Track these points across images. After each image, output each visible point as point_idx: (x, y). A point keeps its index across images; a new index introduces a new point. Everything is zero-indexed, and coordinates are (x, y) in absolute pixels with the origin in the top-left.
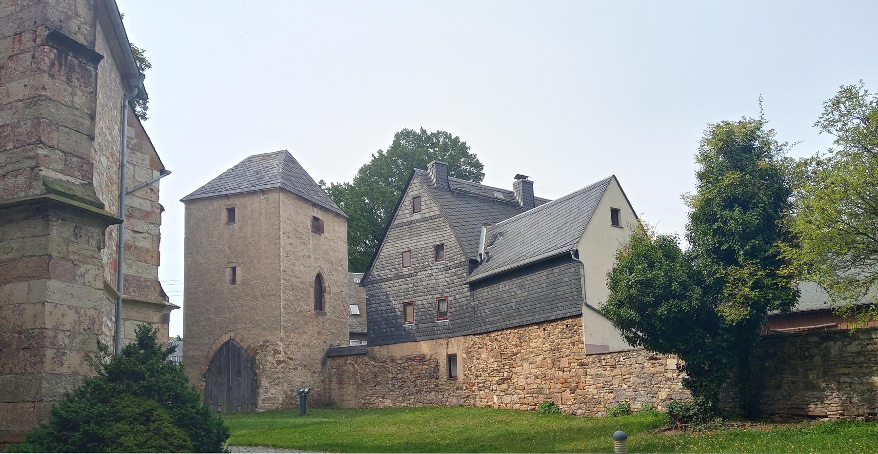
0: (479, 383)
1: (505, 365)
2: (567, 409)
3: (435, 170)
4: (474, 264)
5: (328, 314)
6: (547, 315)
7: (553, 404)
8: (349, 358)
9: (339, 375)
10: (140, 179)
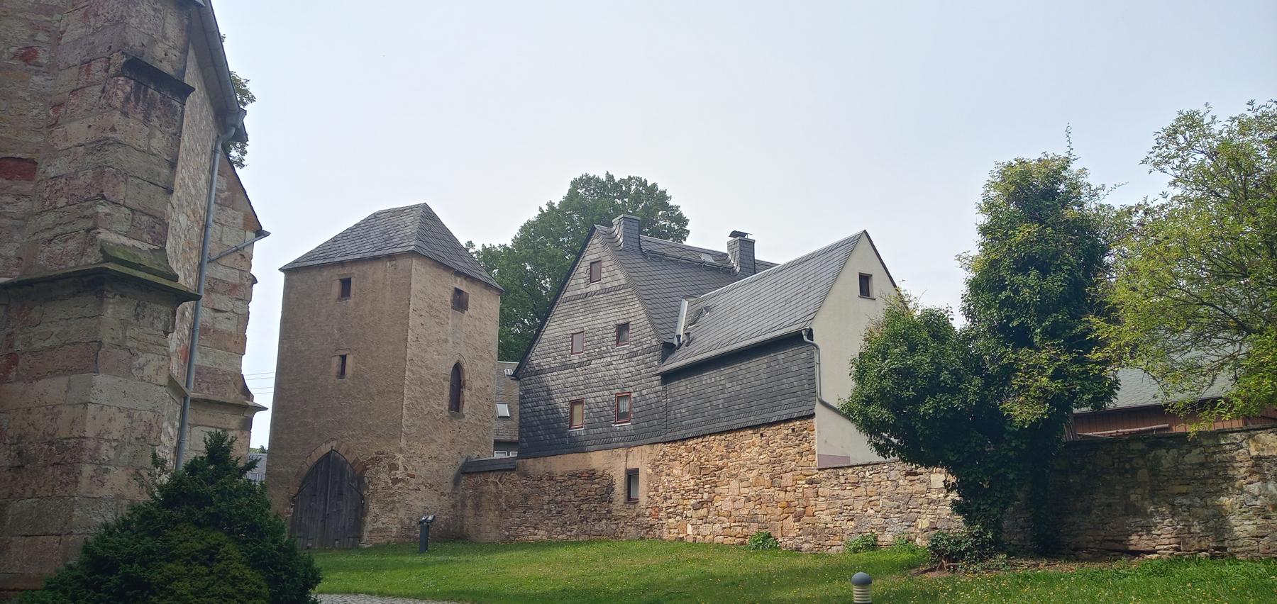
0: (668, 508)
2: (788, 542)
3: (622, 227)
4: (669, 349)
5: (467, 416)
6: (766, 416)
7: (769, 536)
9: (476, 497)
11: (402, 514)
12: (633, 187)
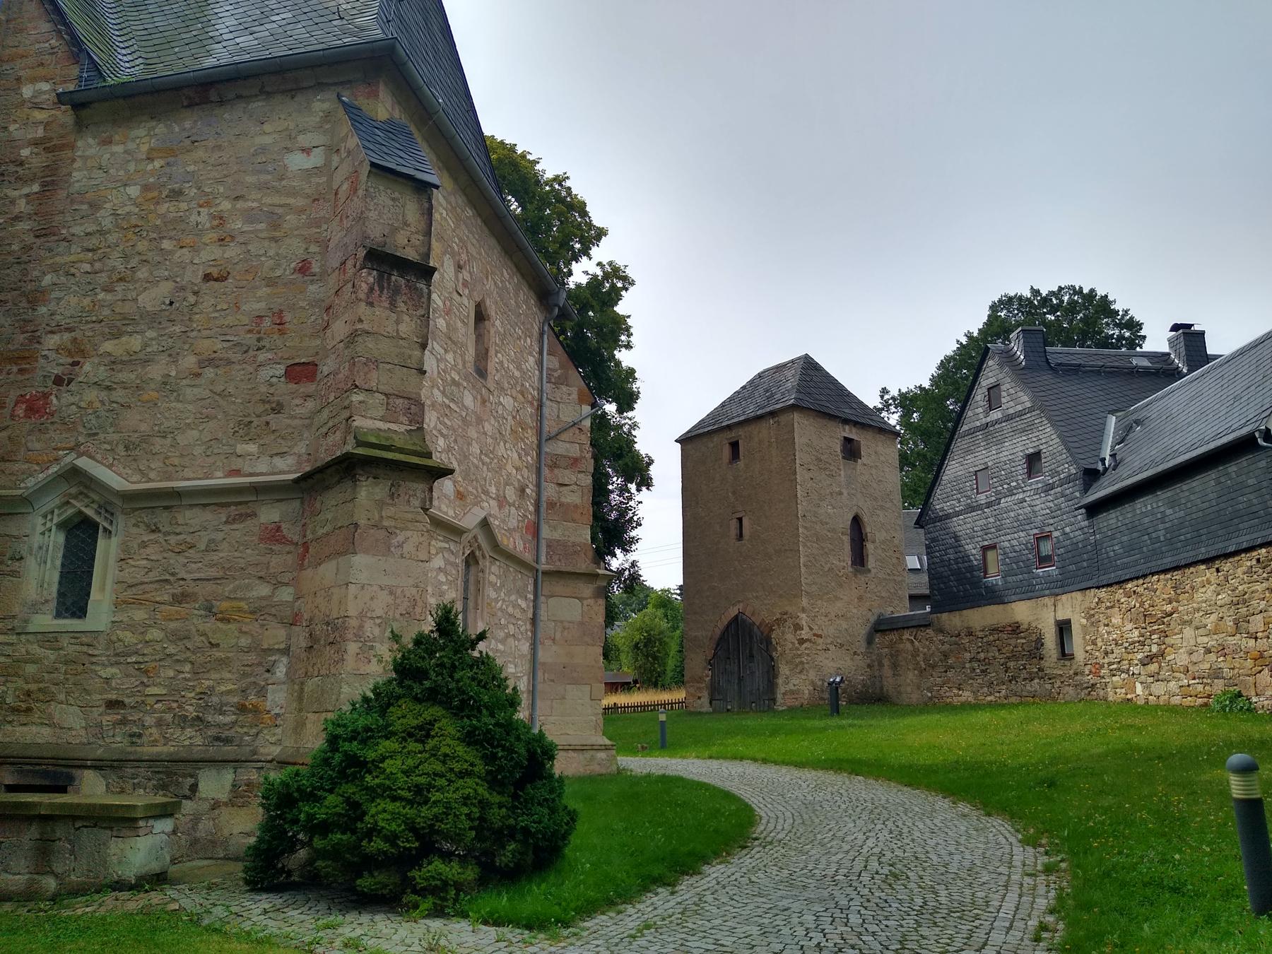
0: (1110, 664)
1: (1152, 633)
2: (1266, 702)
3: (1022, 341)
4: (1091, 476)
5: (873, 571)
6: (1221, 545)
7: (1240, 695)
8: (905, 631)
9: (892, 655)
10: (564, 419)
11: (812, 675)
12: (1066, 298)
